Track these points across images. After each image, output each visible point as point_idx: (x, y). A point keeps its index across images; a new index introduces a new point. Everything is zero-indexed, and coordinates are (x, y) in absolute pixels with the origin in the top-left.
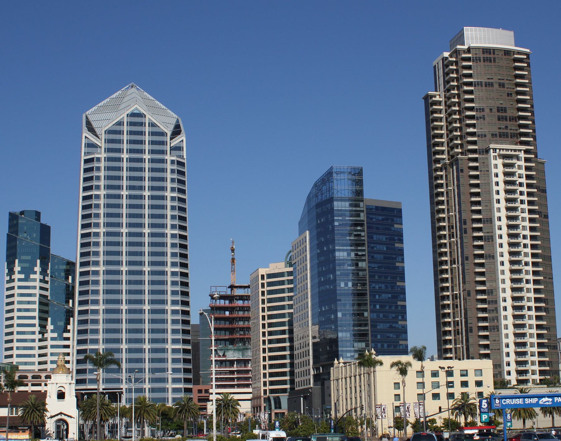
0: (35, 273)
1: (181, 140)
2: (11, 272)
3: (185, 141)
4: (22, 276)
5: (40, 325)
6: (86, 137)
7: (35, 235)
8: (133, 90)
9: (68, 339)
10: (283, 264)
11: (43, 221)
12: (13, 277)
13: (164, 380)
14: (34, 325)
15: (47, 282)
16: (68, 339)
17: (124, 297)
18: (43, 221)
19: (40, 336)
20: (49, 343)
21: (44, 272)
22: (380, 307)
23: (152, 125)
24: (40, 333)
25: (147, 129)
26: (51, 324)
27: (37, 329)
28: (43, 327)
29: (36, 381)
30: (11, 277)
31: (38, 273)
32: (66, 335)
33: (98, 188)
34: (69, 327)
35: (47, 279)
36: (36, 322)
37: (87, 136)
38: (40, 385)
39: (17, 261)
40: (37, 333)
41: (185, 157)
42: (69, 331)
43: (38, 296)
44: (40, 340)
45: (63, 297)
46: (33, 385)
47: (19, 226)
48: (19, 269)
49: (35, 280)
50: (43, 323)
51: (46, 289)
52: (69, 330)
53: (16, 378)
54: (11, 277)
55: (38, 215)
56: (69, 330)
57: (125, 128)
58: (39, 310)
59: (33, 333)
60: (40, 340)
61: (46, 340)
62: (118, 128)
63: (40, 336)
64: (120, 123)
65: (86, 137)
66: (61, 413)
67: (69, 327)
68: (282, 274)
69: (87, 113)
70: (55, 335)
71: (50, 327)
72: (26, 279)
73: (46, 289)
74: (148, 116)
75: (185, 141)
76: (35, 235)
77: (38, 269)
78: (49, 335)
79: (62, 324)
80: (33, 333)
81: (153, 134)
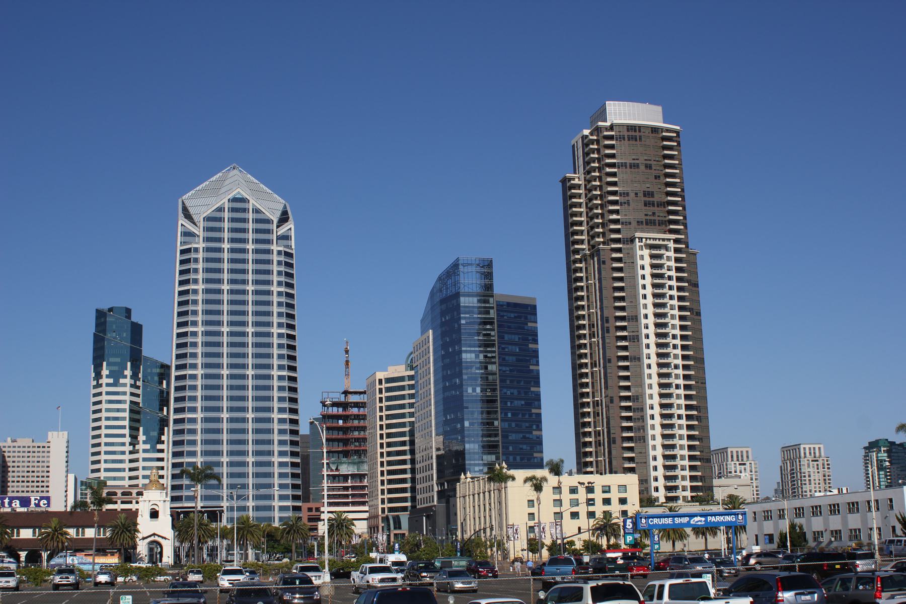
0: (125, 377)
9: (162, 451)
11: (134, 318)
15: (138, 388)
16: (162, 451)
18: (134, 318)
19: (131, 448)
20: (141, 455)
21: (135, 376)
23: (257, 211)
24: (130, 444)
25: (251, 216)
27: (127, 440)
28: (98, 376)
29: (126, 498)
31: (129, 377)
32: (159, 447)
34: (163, 438)
35: (139, 383)
36: (127, 431)
38: (131, 502)
39: (105, 363)
40: (127, 444)
41: (293, 247)
42: (163, 442)
43: (128, 402)
44: (131, 452)
45: (157, 404)
46: (123, 502)
49: (125, 385)
50: (134, 433)
51: (138, 396)
55: (128, 312)
59: (123, 444)
61: (137, 452)
62: (218, 215)
63: (131, 448)
64: (220, 209)
66: (154, 534)
67: (163, 438)
68: (402, 379)
72: (115, 384)
73: (138, 396)
74: (252, 201)
77: (128, 372)
78: (104, 381)
80: (123, 444)
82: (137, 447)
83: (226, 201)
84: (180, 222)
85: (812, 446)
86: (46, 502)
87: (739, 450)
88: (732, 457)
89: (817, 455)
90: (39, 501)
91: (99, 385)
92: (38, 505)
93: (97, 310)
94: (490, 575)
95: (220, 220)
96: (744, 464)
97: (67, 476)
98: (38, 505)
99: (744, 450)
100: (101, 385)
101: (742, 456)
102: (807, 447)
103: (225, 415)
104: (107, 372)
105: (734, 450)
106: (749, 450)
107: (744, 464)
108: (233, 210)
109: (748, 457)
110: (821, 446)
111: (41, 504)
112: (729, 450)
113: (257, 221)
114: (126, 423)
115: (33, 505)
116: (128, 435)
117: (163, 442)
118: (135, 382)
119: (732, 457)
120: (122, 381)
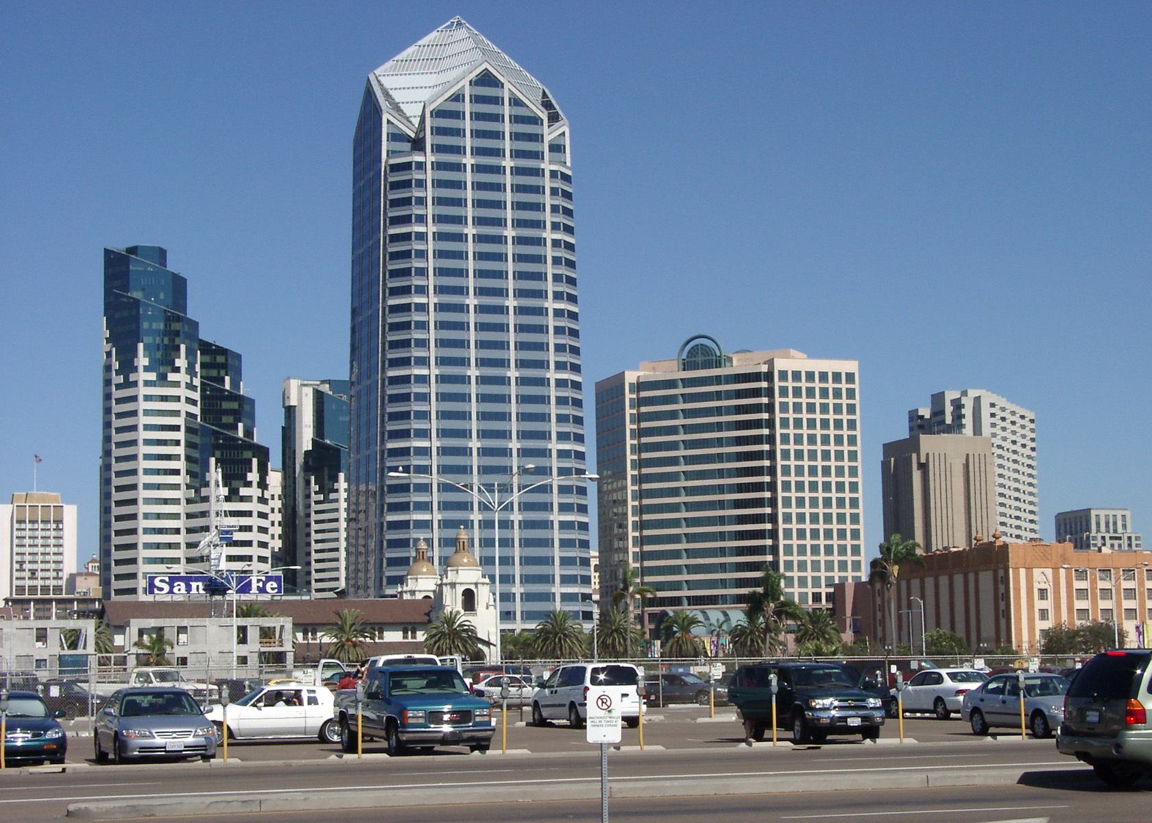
1: (560, 131)
2: (128, 366)
3: (567, 134)
6: (389, 121)
7: (162, 296)
8: (462, 33)
10: (674, 365)
11: (171, 267)
12: (132, 377)
13: (548, 579)
14: (176, 472)
17: (474, 425)
18: (171, 267)
23: (516, 102)
24: (188, 487)
25: (507, 110)
30: (126, 378)
33: (421, 219)
37: (392, 119)
39: (141, 346)
41: (569, 164)
43: (183, 415)
47: (132, 276)
49: (176, 384)
50: (196, 468)
52: (251, 483)
54: (126, 378)
55: (162, 253)
56: (251, 483)
57: (467, 107)
58: (186, 441)
59: (176, 487)
62: (454, 107)
64: (458, 98)
65: (389, 121)
68: (671, 384)
69: (377, 72)
72: (162, 378)
74: (507, 86)
75: (567, 134)
76: (162, 296)
80: (176, 487)
81: (516, 119)
83: (466, 82)
84: (385, 117)
85: (1111, 513)
86: (275, 585)
87: (1111, 513)
88: (1098, 524)
89: (1120, 529)
90: (264, 584)
91: (129, 384)
92: (262, 590)
93: (107, 252)
94: (855, 722)
95: (458, 115)
96: (1120, 538)
98: (262, 590)
99: (1119, 514)
101: (1115, 523)
102: (1102, 513)
103: (475, 444)
105: (1102, 513)
106: (1127, 513)
107: (1120, 538)
108: (477, 99)
109: (1124, 526)
110: (1127, 513)
111: (268, 589)
112: (1093, 513)
113: (516, 119)
115: (254, 590)
116: (183, 472)
119: (1098, 524)
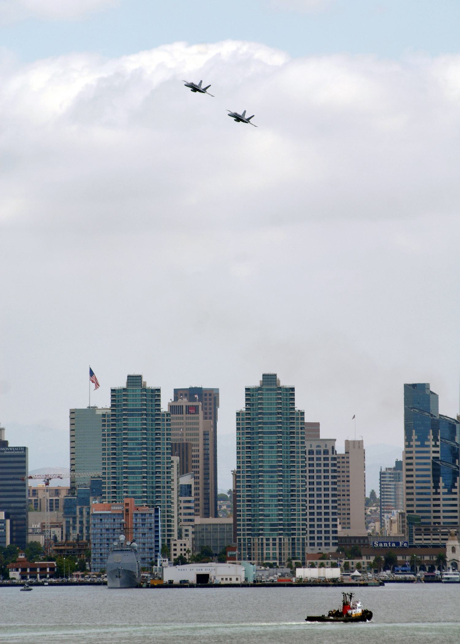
0: (429, 440)
4: (419, 443)
5: (434, 482)
9: (456, 493)
12: (439, 491)
15: (438, 446)
16: (456, 493)
19: (434, 491)
20: (441, 496)
21: (435, 439)
22: (50, 570)
24: (434, 488)
26: (443, 482)
27: (432, 485)
28: (436, 487)
29: (427, 532)
31: (431, 440)
32: (454, 490)
34: (456, 484)
35: (438, 443)
36: (431, 479)
38: (430, 535)
39: (441, 478)
40: (432, 488)
42: (456, 487)
44: (434, 494)
45: (450, 459)
46: (425, 535)
48: (443, 485)
51: (438, 452)
53: (229, 556)
60: (434, 494)
61: (439, 493)
63: (434, 491)
66: (454, 560)
67: (456, 484)
70: (446, 490)
71: (441, 484)
72: (423, 445)
73: (438, 452)
77: (431, 437)
78: (441, 490)
79: (450, 482)
80: (429, 488)
82: (439, 491)
97: (170, 585)
100: (439, 493)
104: (416, 437)
114: (430, 473)
117: (456, 487)
118: (436, 491)
120: (426, 443)
